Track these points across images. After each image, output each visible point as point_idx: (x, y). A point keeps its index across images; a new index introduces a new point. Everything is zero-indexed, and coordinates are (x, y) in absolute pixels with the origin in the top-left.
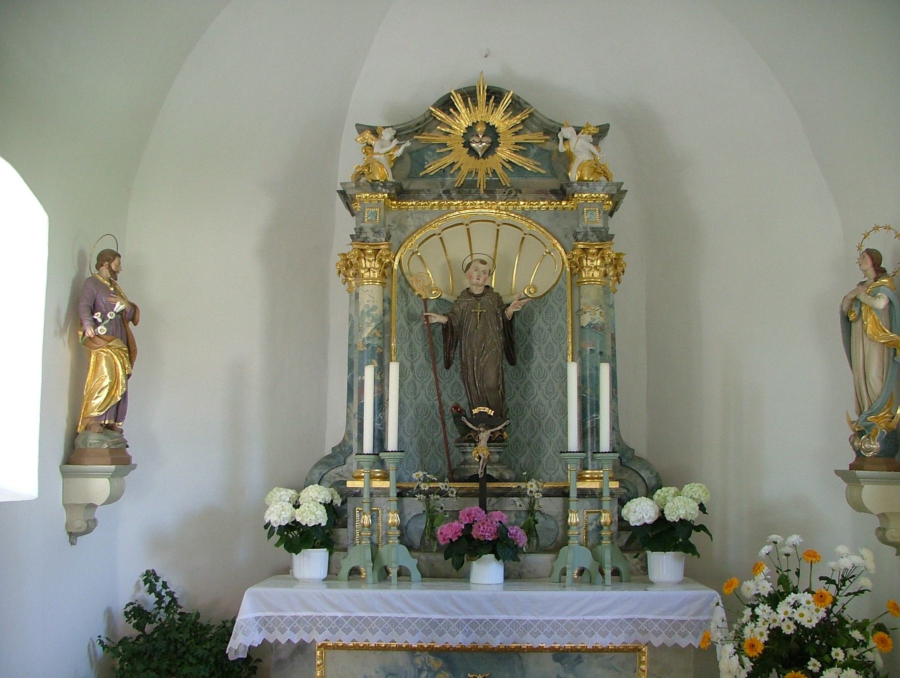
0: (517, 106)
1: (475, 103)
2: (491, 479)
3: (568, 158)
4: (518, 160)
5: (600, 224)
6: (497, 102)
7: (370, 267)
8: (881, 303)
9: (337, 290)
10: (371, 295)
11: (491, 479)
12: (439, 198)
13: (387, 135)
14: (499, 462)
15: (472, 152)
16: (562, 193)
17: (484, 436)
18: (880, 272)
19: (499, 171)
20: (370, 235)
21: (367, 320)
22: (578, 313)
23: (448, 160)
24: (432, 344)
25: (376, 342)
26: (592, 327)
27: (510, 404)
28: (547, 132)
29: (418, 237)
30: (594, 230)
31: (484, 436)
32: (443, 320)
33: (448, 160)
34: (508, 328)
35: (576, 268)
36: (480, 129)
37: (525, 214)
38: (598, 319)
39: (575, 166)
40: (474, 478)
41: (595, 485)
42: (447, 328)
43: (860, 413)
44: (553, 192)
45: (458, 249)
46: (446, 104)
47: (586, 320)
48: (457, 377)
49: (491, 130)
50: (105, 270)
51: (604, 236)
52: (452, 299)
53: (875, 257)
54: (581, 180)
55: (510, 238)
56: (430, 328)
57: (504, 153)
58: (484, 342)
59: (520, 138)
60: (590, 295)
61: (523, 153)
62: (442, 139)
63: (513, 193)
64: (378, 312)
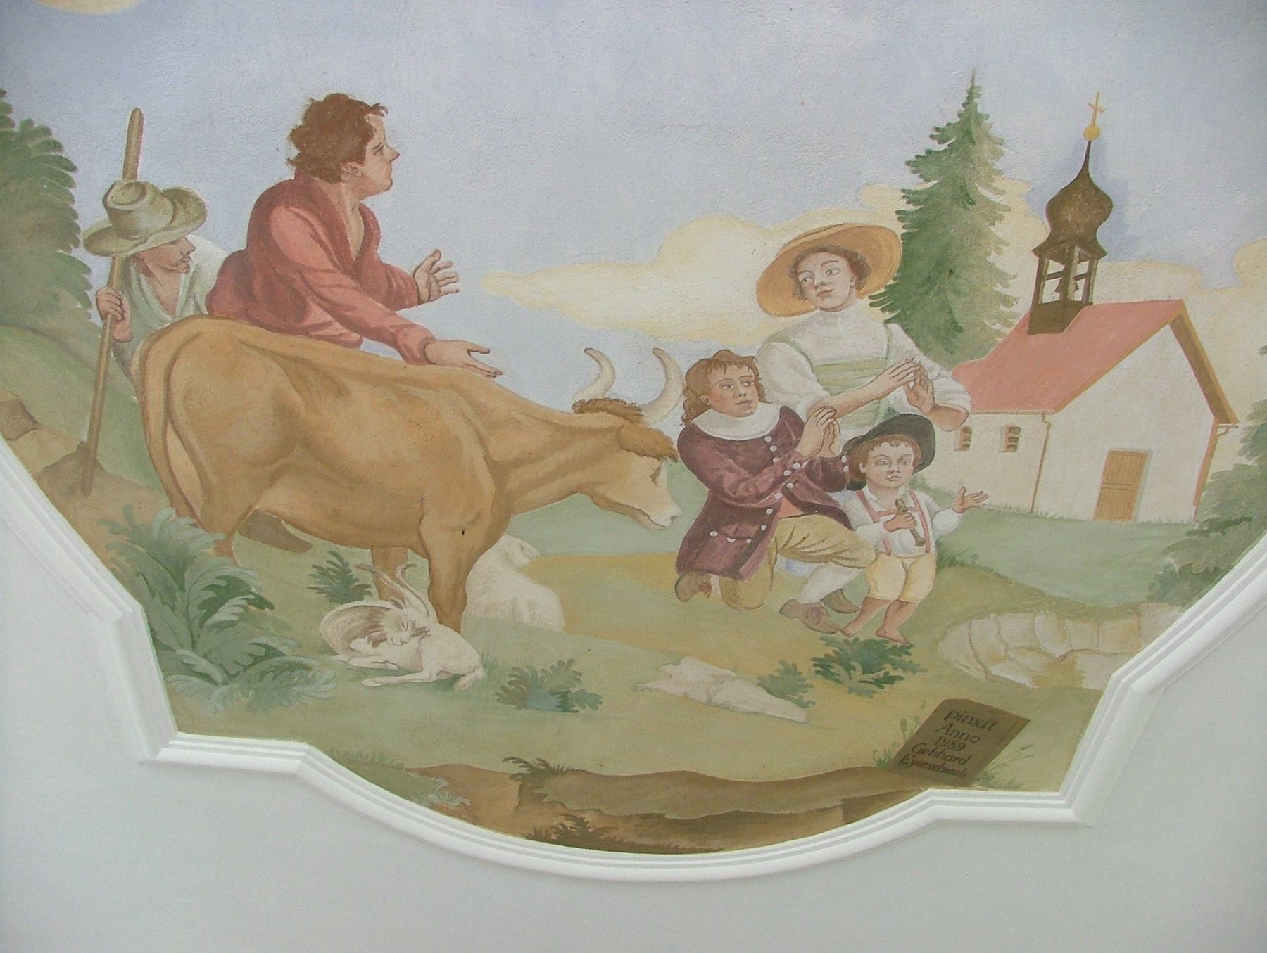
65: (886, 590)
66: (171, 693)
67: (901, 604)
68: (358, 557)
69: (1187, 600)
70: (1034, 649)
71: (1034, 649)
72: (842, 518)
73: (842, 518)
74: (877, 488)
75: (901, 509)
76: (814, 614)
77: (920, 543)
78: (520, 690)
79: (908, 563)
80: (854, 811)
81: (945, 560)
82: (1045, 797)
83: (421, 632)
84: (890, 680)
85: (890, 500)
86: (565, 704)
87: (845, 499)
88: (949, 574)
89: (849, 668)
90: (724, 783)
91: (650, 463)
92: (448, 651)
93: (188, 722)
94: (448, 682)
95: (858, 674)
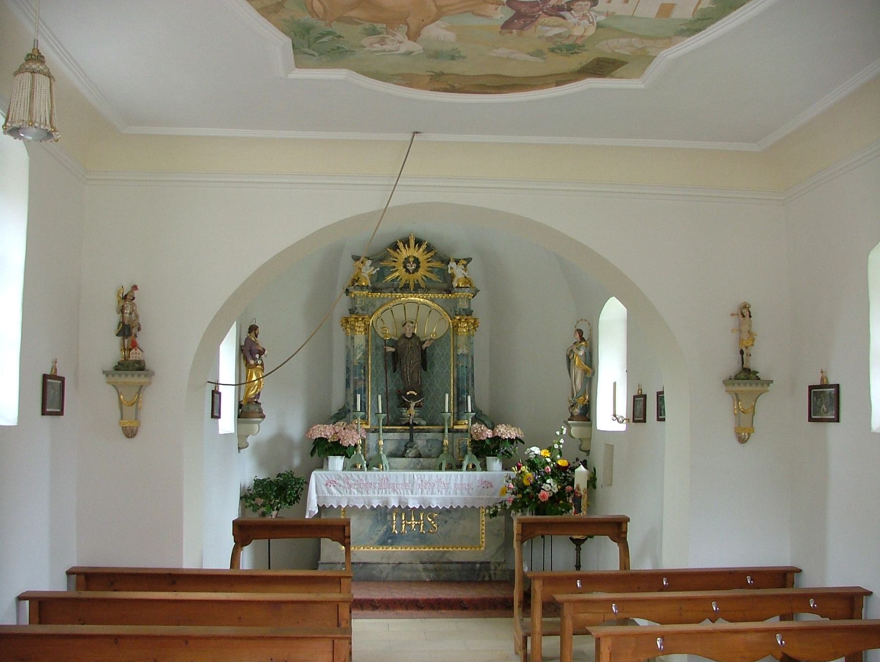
0: (429, 249)
1: (409, 247)
2: (415, 425)
3: (452, 276)
4: (429, 275)
5: (467, 307)
6: (420, 246)
7: (360, 326)
8: (581, 353)
9: (339, 335)
10: (360, 339)
11: (415, 425)
12: (391, 292)
13: (369, 263)
14: (419, 417)
15: (407, 271)
16: (449, 291)
17: (413, 404)
18: (582, 339)
19: (420, 280)
20: (360, 311)
21: (358, 351)
22: (456, 348)
23: (397, 274)
24: (385, 360)
25: (362, 361)
26: (463, 355)
27: (424, 389)
28: (442, 261)
29: (381, 310)
30: (464, 310)
31: (413, 404)
32: (393, 350)
33: (397, 274)
34: (424, 353)
35: (456, 327)
36: (411, 259)
37: (432, 300)
38: (465, 351)
39: (455, 280)
40: (408, 424)
41: (465, 427)
42: (394, 354)
43: (573, 397)
44: (446, 291)
45: (399, 313)
46: (395, 247)
47: (460, 352)
48: (398, 376)
49: (417, 261)
50: (253, 334)
51: (469, 313)
52: (396, 339)
53: (580, 332)
54: (458, 287)
55: (423, 311)
56: (386, 354)
57: (421, 272)
58: (412, 361)
59: (430, 264)
60: (462, 339)
61: (431, 272)
62: (393, 264)
63: (427, 290)
64: (363, 347)
65: (577, 32)
66: (295, 59)
67: (582, 36)
68: (379, 26)
69: (689, 36)
70: (632, 46)
71: (632, 46)
72: (564, 18)
73: (564, 18)
74: (575, 11)
75: (584, 16)
76: (549, 39)
77: (590, 23)
78: (436, 55)
79: (487, 579)
80: (558, 84)
81: (599, 26)
82: (634, 81)
83: (401, 42)
84: (576, 53)
85: (581, 14)
86: (453, 58)
87: (566, 14)
88: (600, 30)
89: (561, 51)
90: (510, 77)
91: (494, 6)
92: (409, 45)
93: (299, 65)
94: (409, 53)
95: (565, 52)
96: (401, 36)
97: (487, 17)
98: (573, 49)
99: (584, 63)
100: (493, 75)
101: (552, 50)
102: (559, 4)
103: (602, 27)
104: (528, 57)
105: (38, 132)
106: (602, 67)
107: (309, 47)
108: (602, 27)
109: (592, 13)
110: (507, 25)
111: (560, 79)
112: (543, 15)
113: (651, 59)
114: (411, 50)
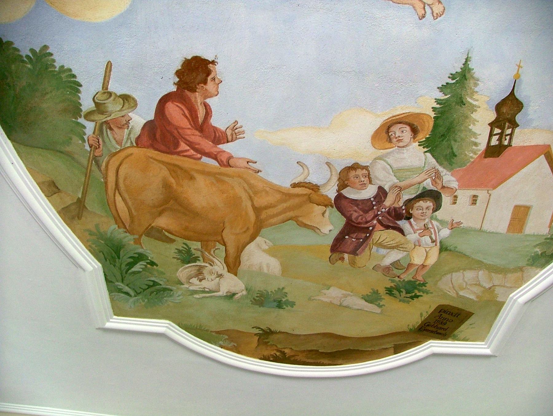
65: (418, 260)
67: (423, 266)
68: (195, 246)
69: (543, 266)
71: (479, 285)
72: (401, 231)
73: (401, 231)
77: (433, 241)
78: (260, 300)
80: (398, 349)
81: (443, 249)
83: (220, 276)
85: (422, 224)
86: (280, 305)
88: (444, 254)
89: (400, 292)
92: (231, 283)
93: (118, 312)
94: (231, 296)
95: (404, 294)
96: (220, 267)
97: (313, 228)
98: (410, 290)
99: (425, 315)
100: (325, 335)
101: (390, 291)
102: (396, 205)
103: (446, 249)
104: (363, 302)
105: (21, 132)
106: (444, 322)
107: (204, 262)
108: (446, 249)
109: (435, 223)
110: (337, 246)
111: (400, 342)
112: (379, 227)
113: (500, 305)
114: (233, 290)
